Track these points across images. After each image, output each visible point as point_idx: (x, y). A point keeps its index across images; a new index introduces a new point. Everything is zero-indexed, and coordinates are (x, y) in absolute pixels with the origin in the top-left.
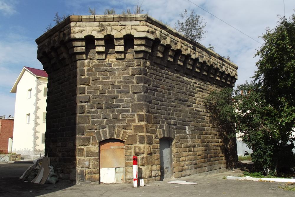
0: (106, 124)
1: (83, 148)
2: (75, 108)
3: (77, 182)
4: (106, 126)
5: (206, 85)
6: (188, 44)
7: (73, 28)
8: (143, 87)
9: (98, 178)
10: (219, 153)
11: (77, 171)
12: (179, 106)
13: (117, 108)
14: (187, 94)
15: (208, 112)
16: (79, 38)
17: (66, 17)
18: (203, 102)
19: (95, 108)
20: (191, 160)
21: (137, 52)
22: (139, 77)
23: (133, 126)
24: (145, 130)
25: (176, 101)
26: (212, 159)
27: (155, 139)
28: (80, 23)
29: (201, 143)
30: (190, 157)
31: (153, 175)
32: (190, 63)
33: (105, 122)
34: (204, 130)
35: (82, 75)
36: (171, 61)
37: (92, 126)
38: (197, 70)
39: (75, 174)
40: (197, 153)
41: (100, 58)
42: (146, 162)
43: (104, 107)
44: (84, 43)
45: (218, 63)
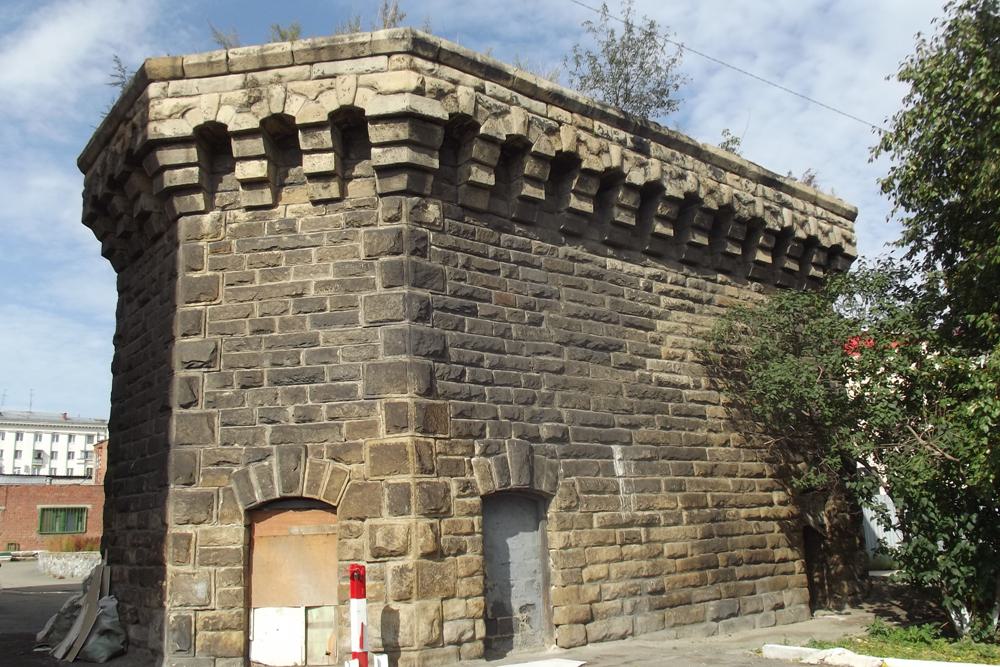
0: (273, 444)
1: (189, 532)
2: (168, 389)
3: (167, 658)
4: (270, 450)
5: (710, 285)
6: (607, 128)
7: (156, 102)
8: (408, 299)
9: (240, 644)
10: (773, 548)
11: (166, 621)
12: (578, 369)
13: (313, 382)
14: (616, 323)
15: (720, 386)
16: (173, 135)
17: (137, 70)
18: (693, 349)
19: (235, 384)
20: (636, 577)
21: (385, 171)
22: (391, 262)
23: (368, 450)
24: (412, 462)
25: (566, 349)
26: (739, 571)
27: (459, 496)
28: (181, 82)
29: (686, 509)
30: (631, 565)
31: (446, 638)
32: (625, 202)
33: (268, 434)
34: (701, 456)
35: (193, 267)
36: (537, 196)
37: (222, 450)
38: (659, 228)
39: (161, 630)
40: (667, 549)
41: (253, 204)
42: (414, 585)
43: (266, 379)
44: (193, 154)
45: (756, 201)
